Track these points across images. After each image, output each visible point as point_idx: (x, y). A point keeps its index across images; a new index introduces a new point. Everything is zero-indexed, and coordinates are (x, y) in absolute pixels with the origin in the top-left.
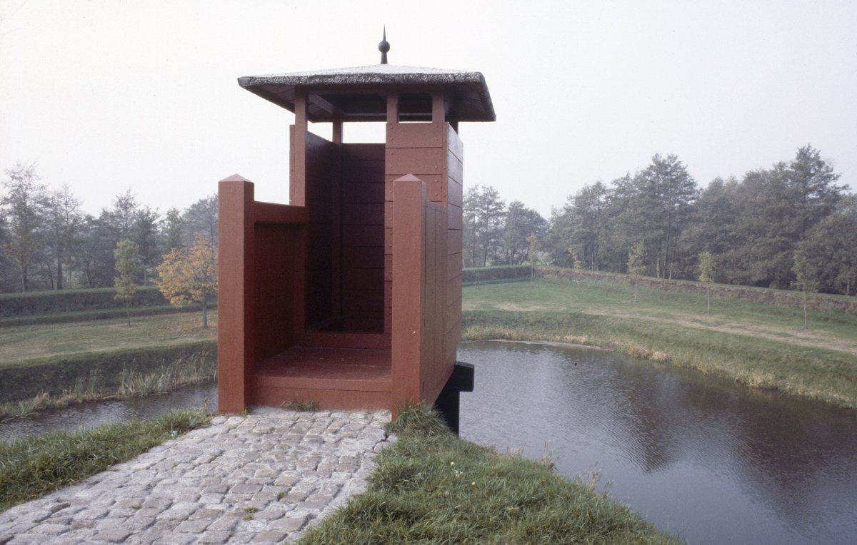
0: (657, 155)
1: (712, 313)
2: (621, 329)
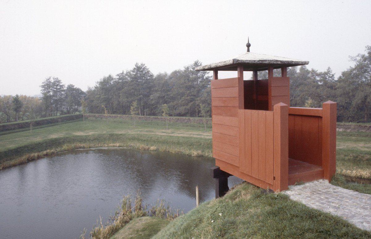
0: (137, 63)
1: (168, 129)
2: (133, 139)
